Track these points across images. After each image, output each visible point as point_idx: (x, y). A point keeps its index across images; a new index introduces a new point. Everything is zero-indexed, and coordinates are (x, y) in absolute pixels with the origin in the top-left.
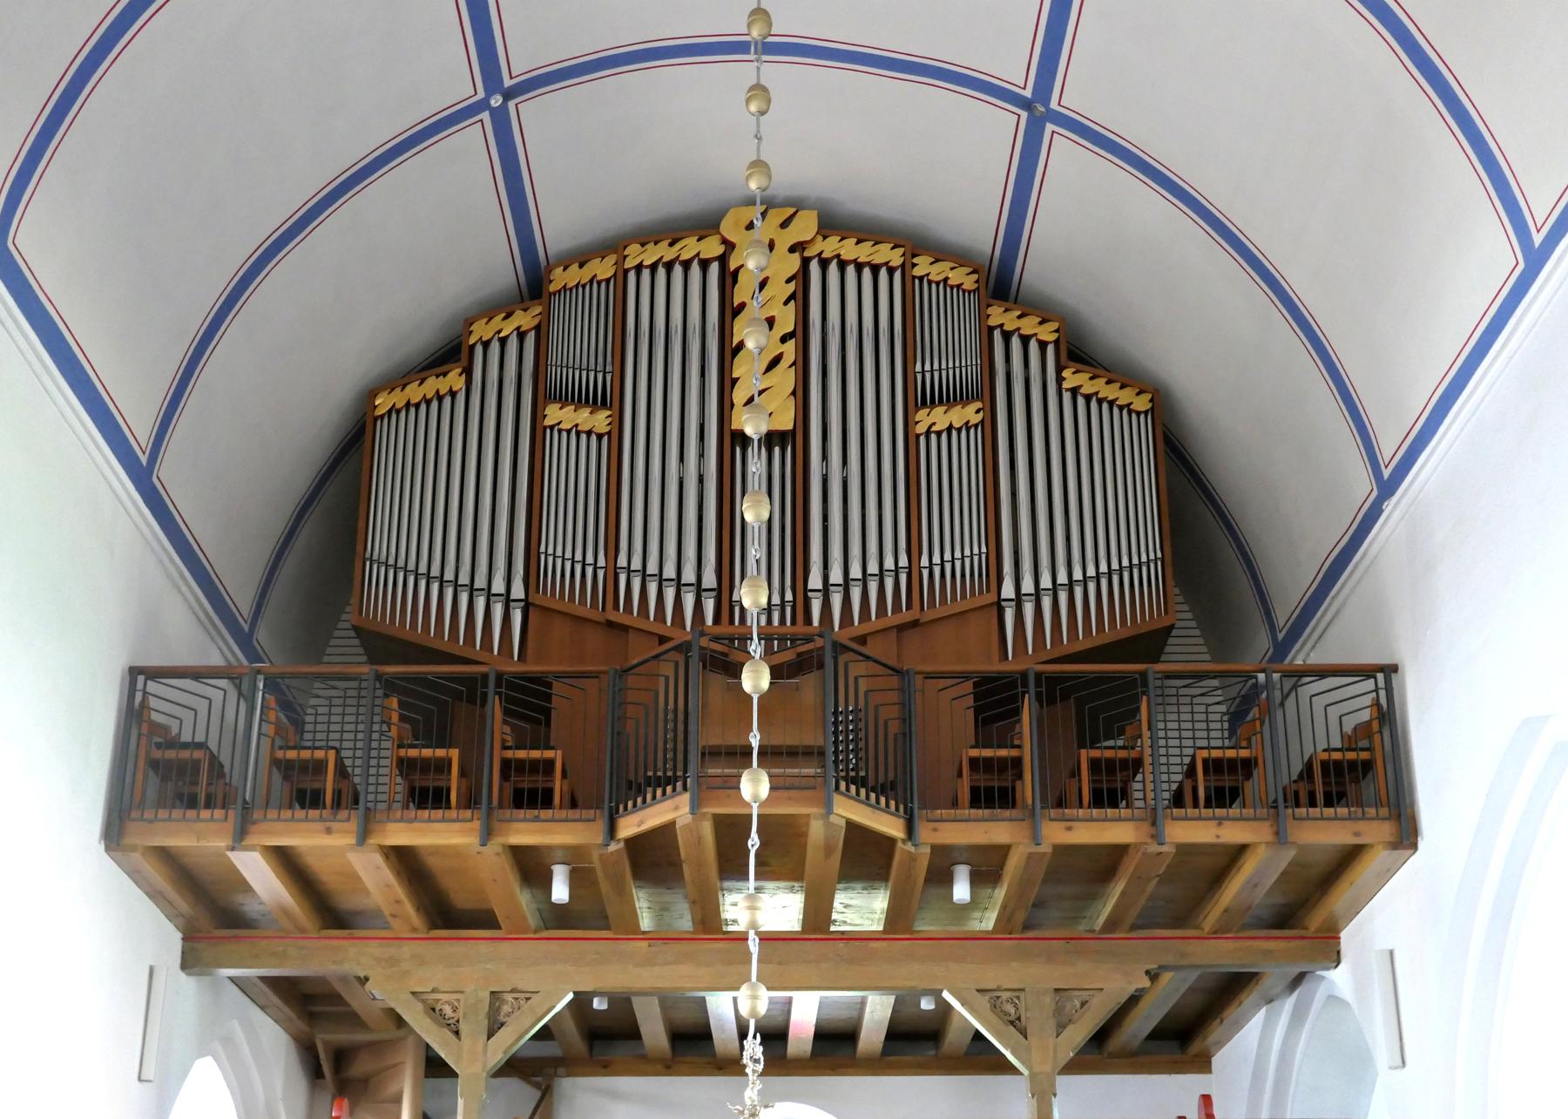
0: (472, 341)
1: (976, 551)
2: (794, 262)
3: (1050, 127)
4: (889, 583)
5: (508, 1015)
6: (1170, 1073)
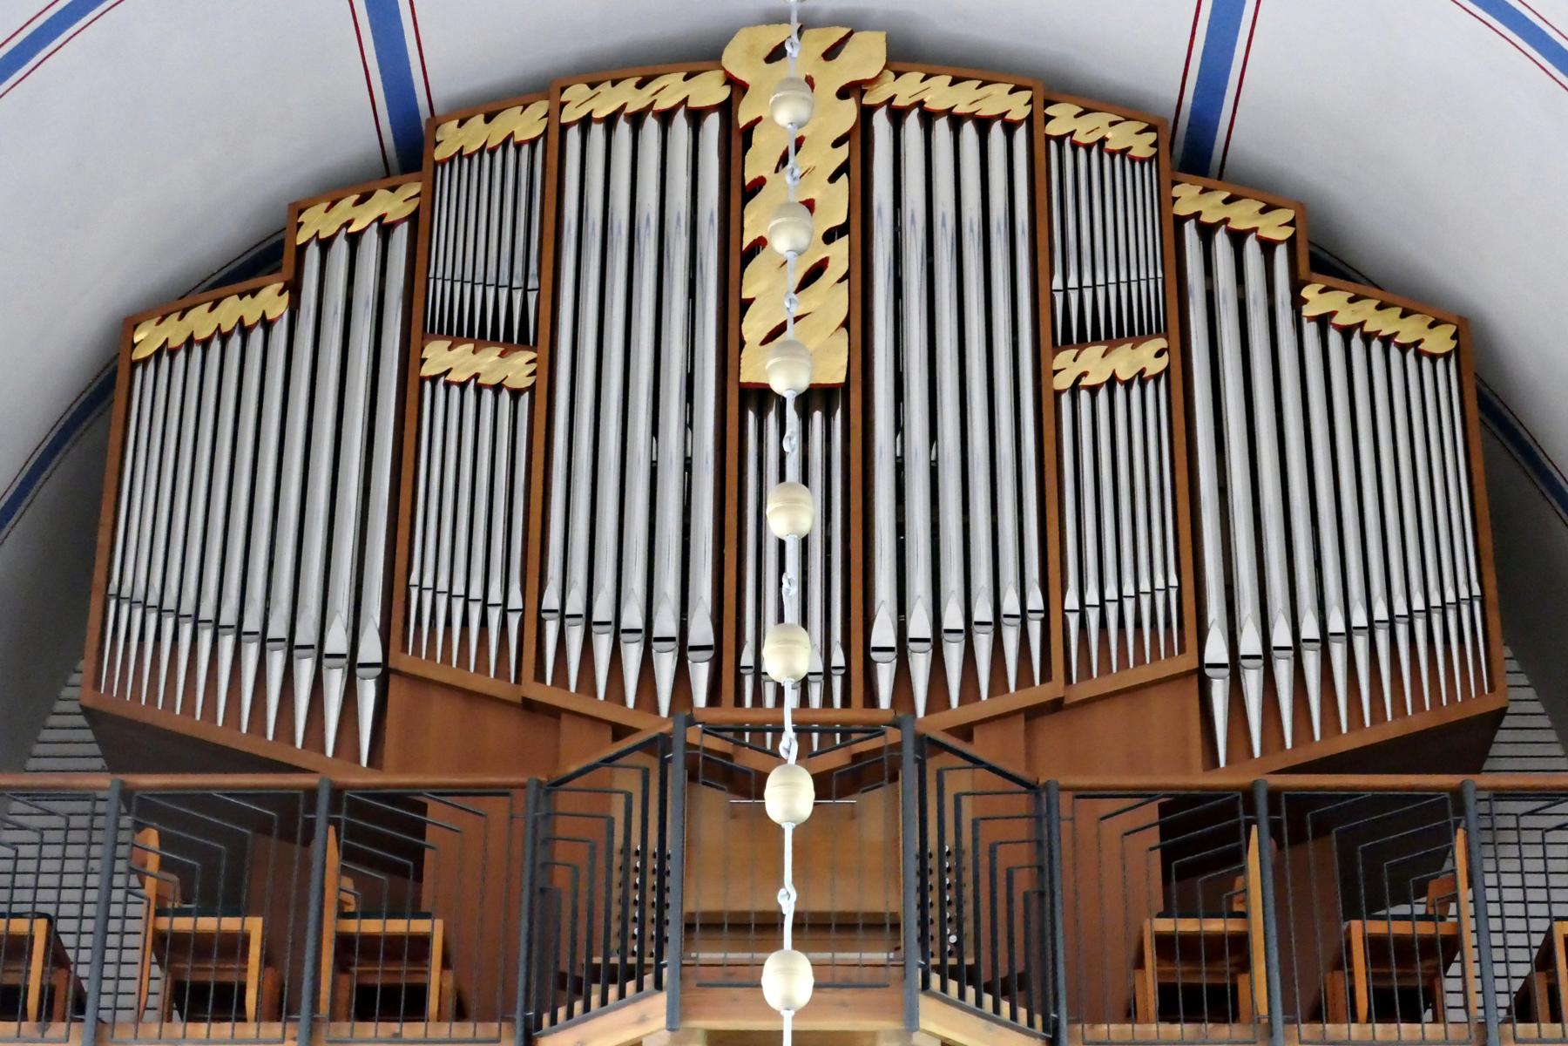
1: (1160, 583)
2: (847, 115)
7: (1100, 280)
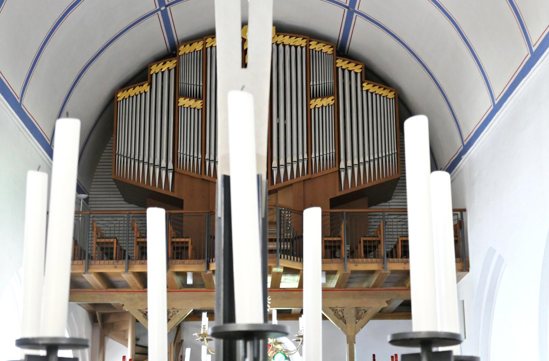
0: (151, 73)
1: (331, 151)
3: (355, 14)
4: (301, 164)
7: (320, 83)
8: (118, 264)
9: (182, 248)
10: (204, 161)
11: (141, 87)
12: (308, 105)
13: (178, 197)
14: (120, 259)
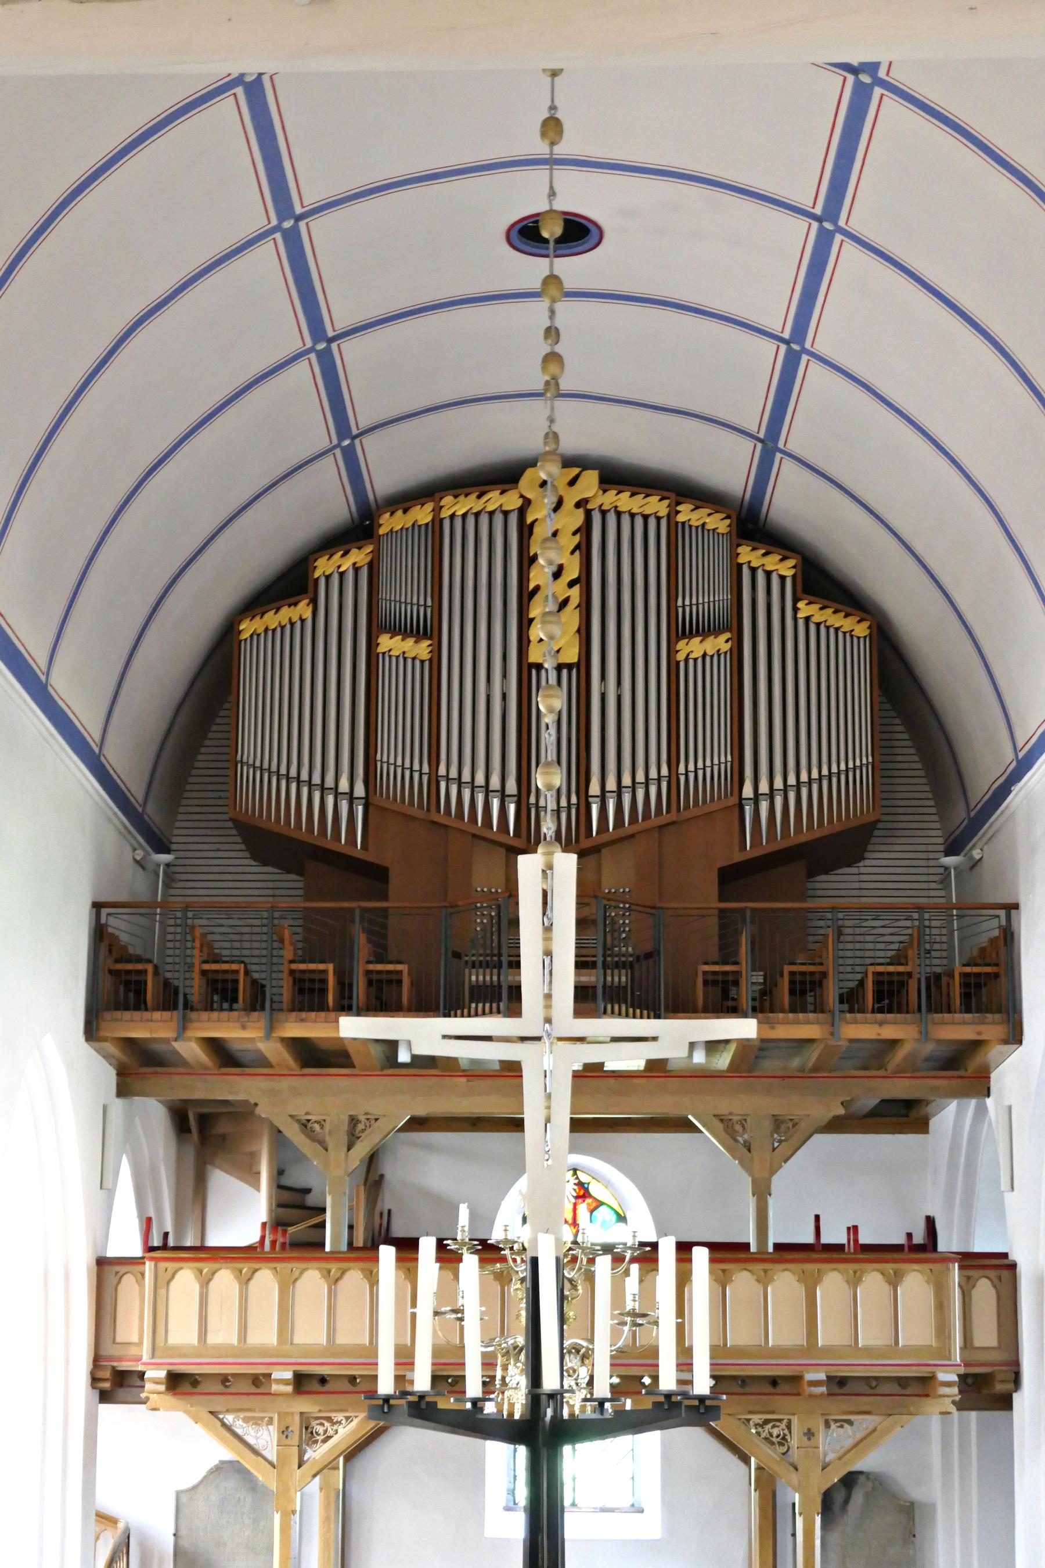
0: (316, 575)
1: (723, 760)
2: (578, 518)
5: (363, 1131)
6: (893, 1133)
7: (701, 601)
8: (248, 1021)
9: (390, 982)
10: (434, 780)
11: (292, 607)
12: (671, 652)
13: (377, 862)
14: (254, 1009)
